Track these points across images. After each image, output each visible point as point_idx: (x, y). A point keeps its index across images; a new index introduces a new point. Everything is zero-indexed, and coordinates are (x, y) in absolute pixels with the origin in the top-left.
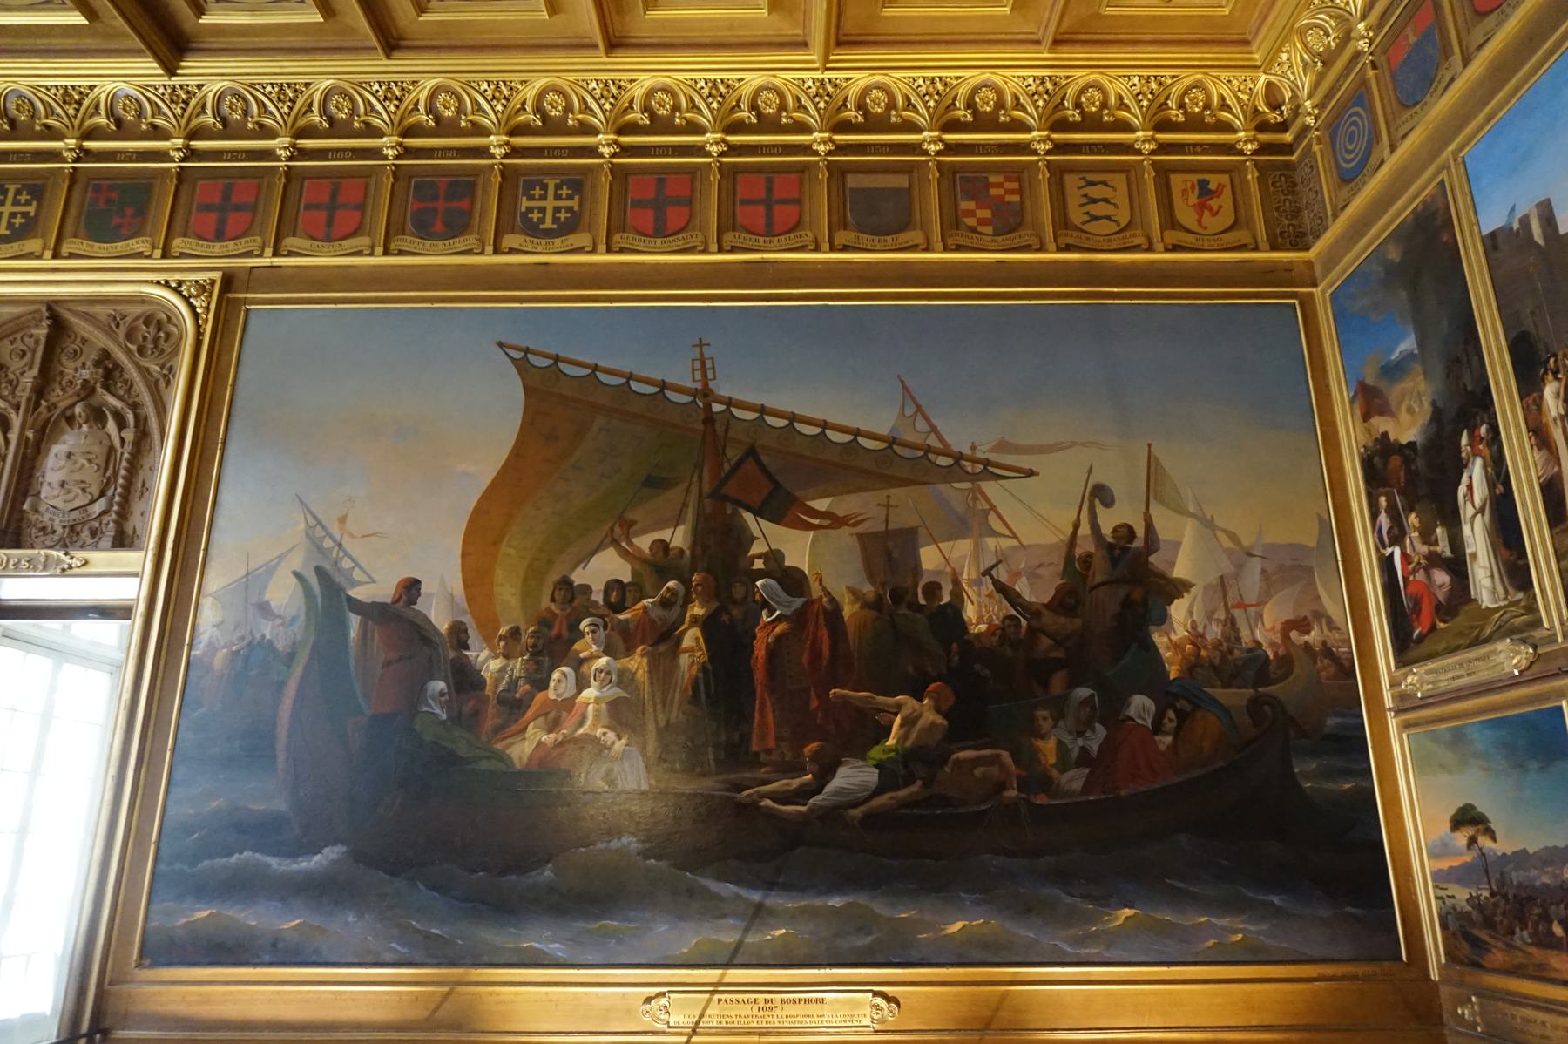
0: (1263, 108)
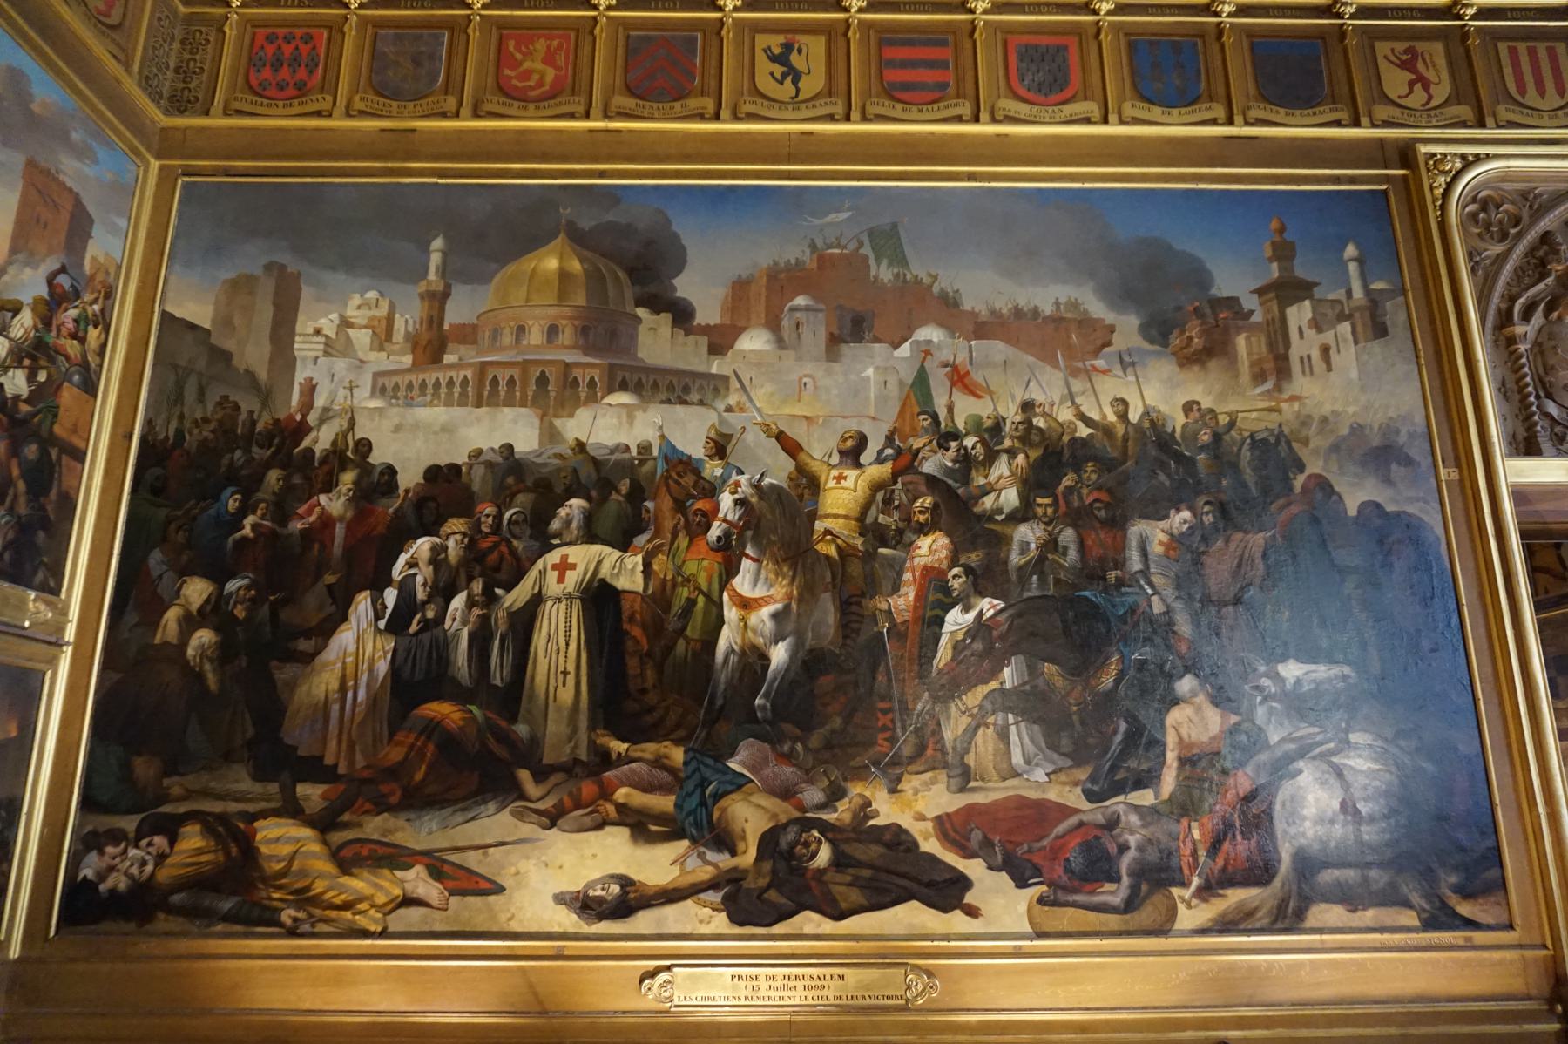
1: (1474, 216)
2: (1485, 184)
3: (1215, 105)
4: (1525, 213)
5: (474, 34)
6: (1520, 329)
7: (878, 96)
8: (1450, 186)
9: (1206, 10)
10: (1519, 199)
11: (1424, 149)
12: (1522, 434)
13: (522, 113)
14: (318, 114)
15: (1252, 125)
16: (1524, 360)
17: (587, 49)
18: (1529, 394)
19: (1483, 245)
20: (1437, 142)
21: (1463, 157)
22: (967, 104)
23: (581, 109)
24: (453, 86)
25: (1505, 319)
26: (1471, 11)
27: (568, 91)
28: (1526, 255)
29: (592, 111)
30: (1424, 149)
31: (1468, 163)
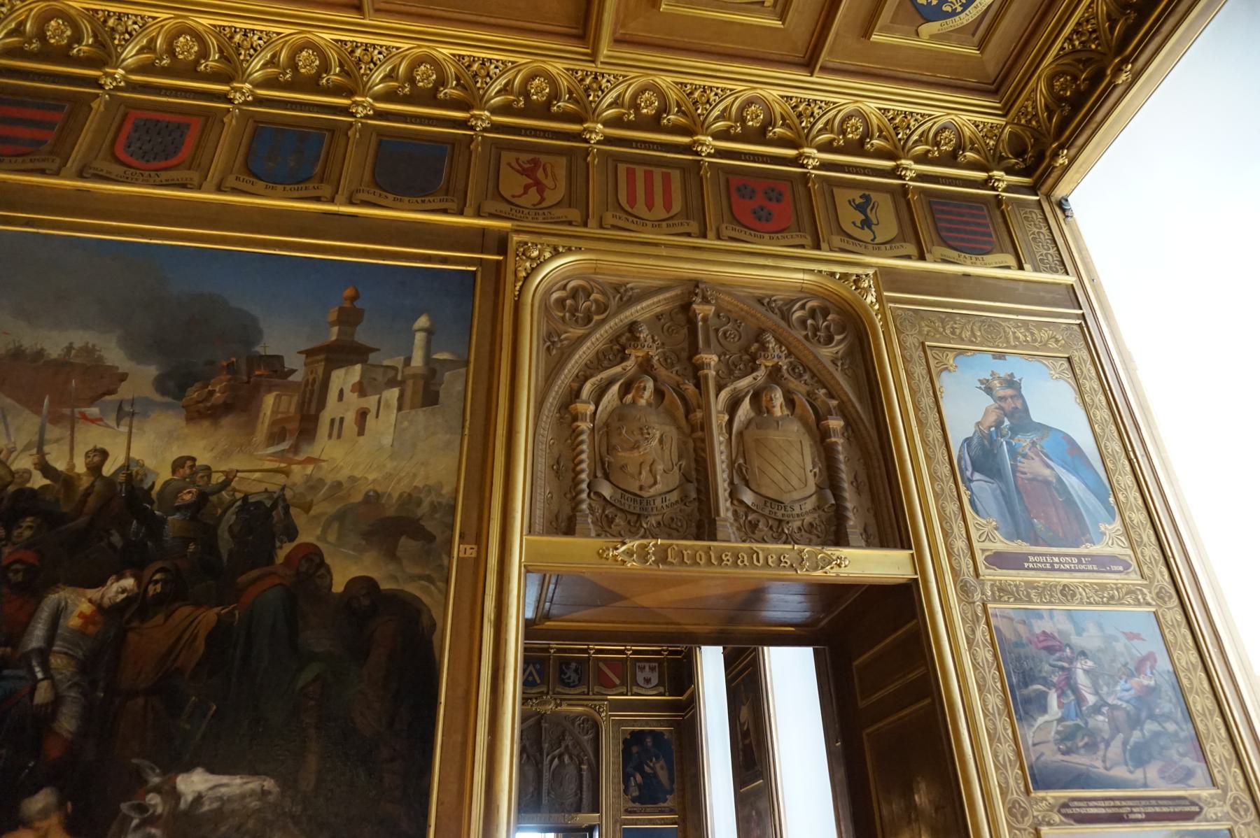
1: (561, 302)
4: (614, 303)
10: (610, 291)
28: (611, 341)
29: (466, 210)
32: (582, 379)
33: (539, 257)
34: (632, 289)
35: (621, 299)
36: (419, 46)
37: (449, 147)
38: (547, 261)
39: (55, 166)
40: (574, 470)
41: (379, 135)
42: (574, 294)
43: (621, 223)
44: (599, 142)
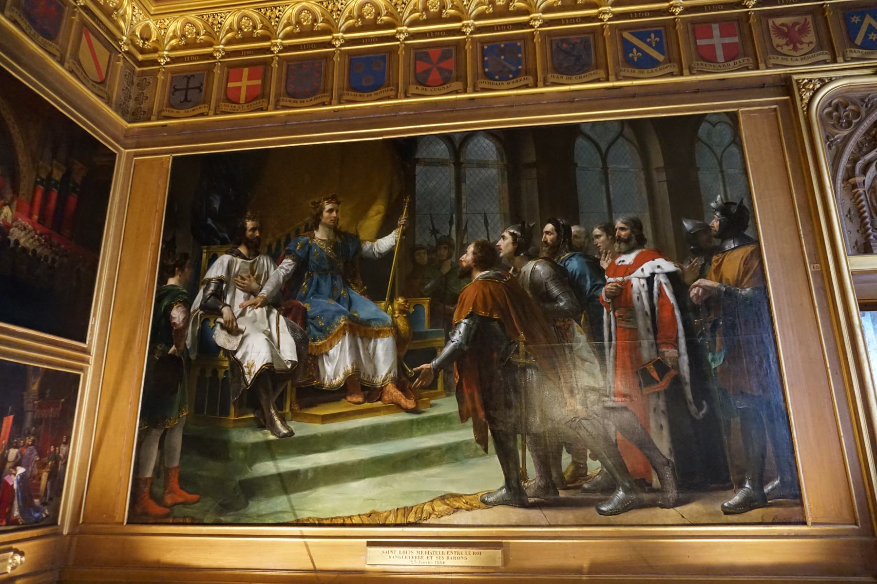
0: (138, 33)
1: (830, 114)
2: (833, 97)
3: (599, 71)
4: (863, 111)
5: (275, 65)
6: (859, 179)
7: (697, 60)
8: (812, 98)
9: (739, 5)
10: (858, 102)
11: (795, 77)
12: (861, 241)
13: (569, 81)
14: (202, 115)
15: (770, 68)
16: (862, 197)
17: (601, 44)
18: (866, 217)
19: (836, 131)
20: (801, 72)
21: (820, 80)
22: (676, 65)
23: (393, 93)
24: (206, 101)
25: (850, 173)
26: (678, 10)
27: (257, 98)
28: (864, 134)
29: (610, 77)
30: (795, 77)
31: (824, 83)
32: (854, 161)
33: (813, 89)
34: (873, 98)
35: (866, 106)
36: (239, 10)
37: (591, 36)
38: (818, 89)
39: (328, 99)
40: (860, 217)
41: (350, 55)
42: (837, 108)
43: (420, 92)
44: (610, 20)
